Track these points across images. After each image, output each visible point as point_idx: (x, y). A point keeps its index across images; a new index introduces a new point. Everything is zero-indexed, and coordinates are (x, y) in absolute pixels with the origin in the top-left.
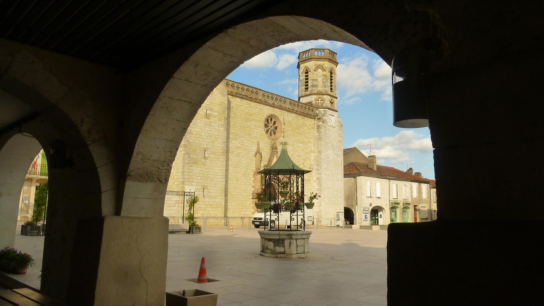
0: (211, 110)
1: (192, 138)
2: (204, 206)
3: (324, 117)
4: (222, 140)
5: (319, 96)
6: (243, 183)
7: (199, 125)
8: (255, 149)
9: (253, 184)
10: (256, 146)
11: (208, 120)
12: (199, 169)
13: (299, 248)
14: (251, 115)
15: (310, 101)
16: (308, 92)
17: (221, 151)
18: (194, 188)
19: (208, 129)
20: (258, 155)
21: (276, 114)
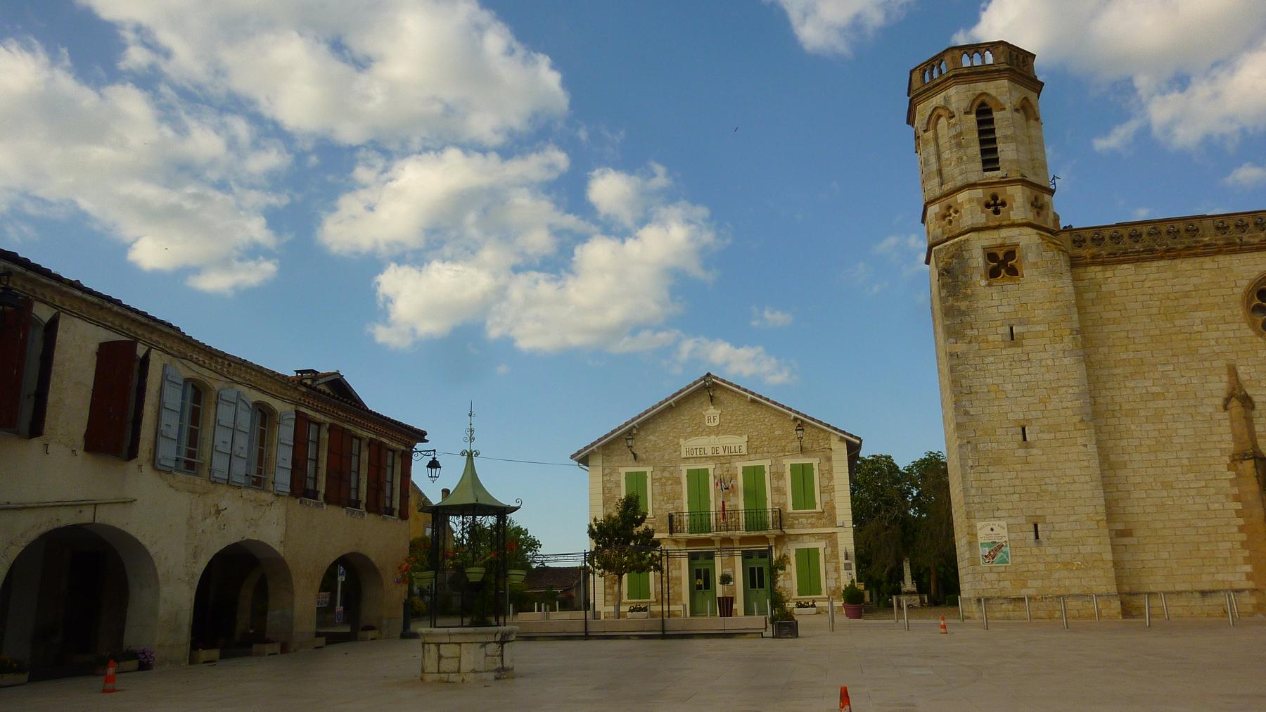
1: (976, 403)
2: (1041, 567)
4: (1076, 390)
6: (1193, 492)
7: (991, 367)
8: (1220, 386)
9: (1235, 491)
10: (1225, 378)
11: (1019, 350)
12: (1013, 475)
13: (443, 661)
14: (1187, 295)
17: (1077, 419)
18: (1004, 523)
19: (1021, 372)
20: (1234, 403)
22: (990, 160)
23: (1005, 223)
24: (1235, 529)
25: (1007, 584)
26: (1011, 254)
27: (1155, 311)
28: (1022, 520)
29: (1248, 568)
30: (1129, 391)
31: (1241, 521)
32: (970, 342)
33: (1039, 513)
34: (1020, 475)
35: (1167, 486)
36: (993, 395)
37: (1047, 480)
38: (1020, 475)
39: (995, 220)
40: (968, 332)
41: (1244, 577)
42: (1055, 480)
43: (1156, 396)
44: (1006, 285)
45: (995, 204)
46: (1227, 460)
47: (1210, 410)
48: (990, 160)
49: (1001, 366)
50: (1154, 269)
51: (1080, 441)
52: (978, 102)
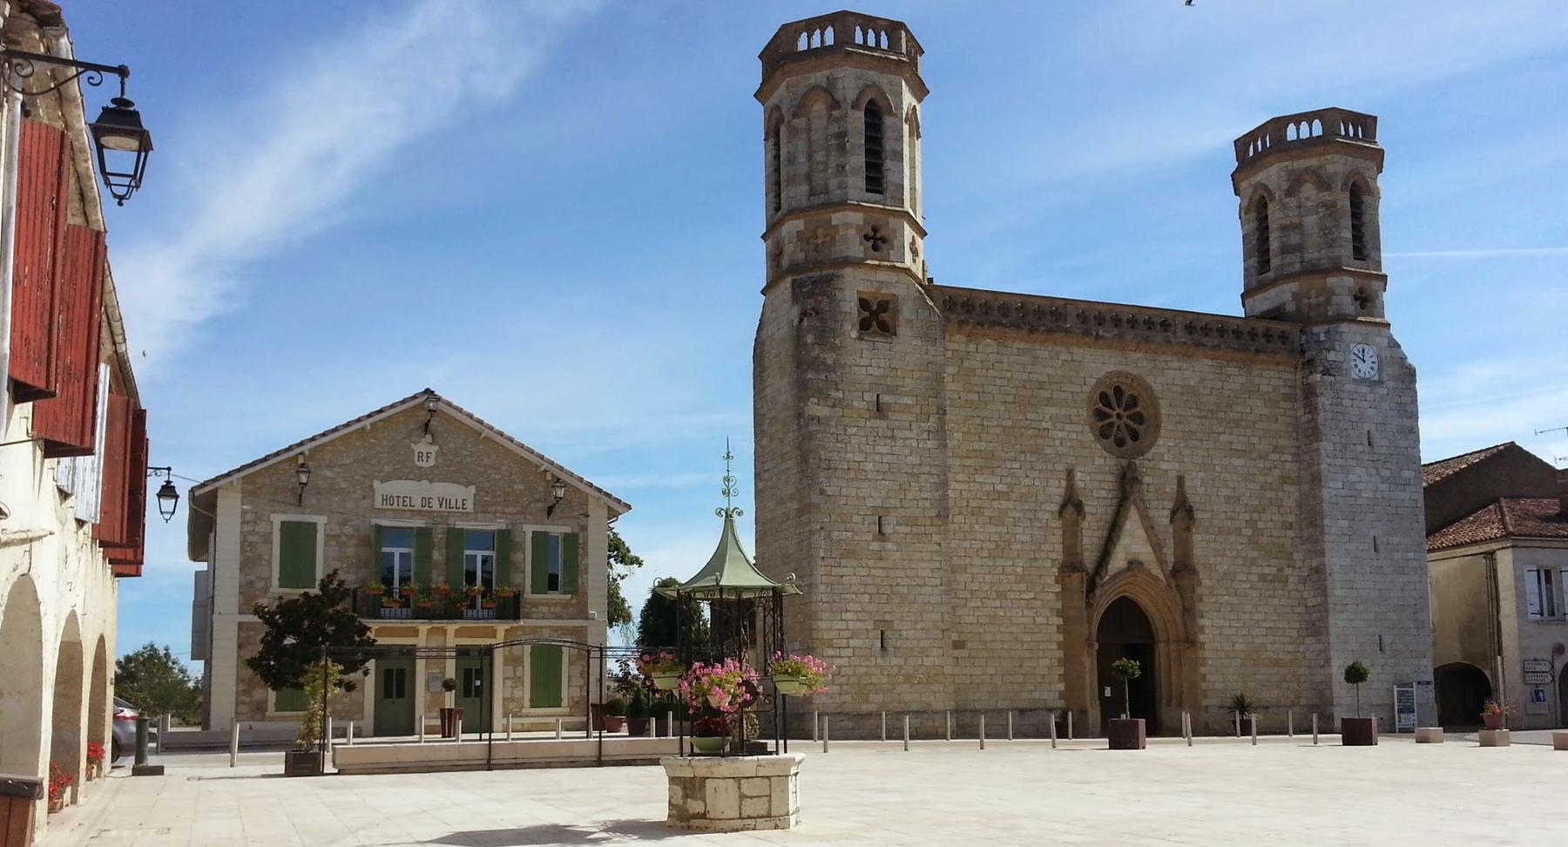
0: (892, 390)
2: (884, 680)
3: (1332, 356)
7: (854, 441)
8: (1057, 490)
10: (1064, 483)
11: (884, 424)
15: (1276, 303)
16: (1270, 275)
19: (885, 450)
20: (1070, 509)
24: (1055, 646)
25: (848, 698)
32: (834, 406)
35: (1001, 595)
36: (852, 474)
40: (834, 394)
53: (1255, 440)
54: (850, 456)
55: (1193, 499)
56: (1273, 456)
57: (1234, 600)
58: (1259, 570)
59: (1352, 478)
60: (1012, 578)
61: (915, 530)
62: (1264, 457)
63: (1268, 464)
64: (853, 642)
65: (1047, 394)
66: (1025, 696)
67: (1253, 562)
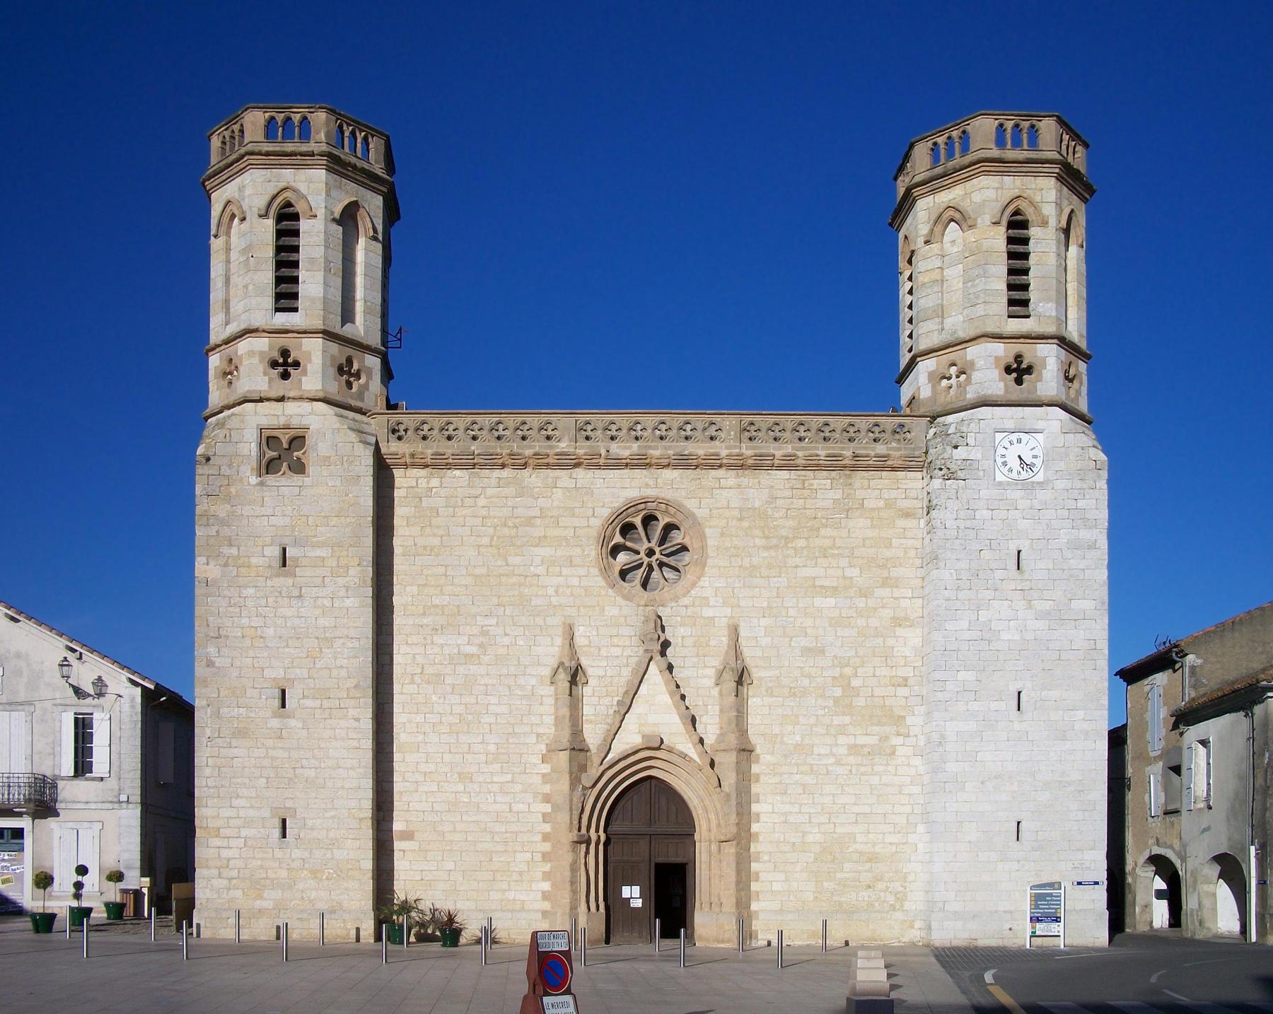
1: (225, 651)
2: (284, 873)
5: (946, 358)
7: (249, 603)
8: (551, 651)
11: (290, 581)
14: (529, 522)
17: (351, 683)
19: (289, 612)
21: (667, 494)
22: (1018, 302)
23: (292, 394)
24: (539, 838)
25: (239, 893)
26: (298, 441)
27: (486, 541)
28: (266, 813)
29: (546, 886)
30: (436, 650)
31: (547, 828)
32: (226, 565)
33: (289, 804)
34: (272, 753)
35: (465, 777)
36: (248, 642)
37: (304, 762)
38: (272, 753)
39: (1017, 393)
40: (227, 551)
41: (539, 896)
42: (313, 762)
43: (469, 656)
44: (284, 482)
45: (285, 364)
46: (543, 748)
47: (533, 681)
48: (1018, 302)
49: (263, 602)
50: (494, 482)
51: (352, 712)
52: (1011, 208)
53: (854, 572)
54: (245, 621)
55: (750, 654)
56: (879, 592)
57: (809, 780)
58: (851, 740)
59: (984, 615)
60: (483, 757)
61: (326, 704)
62: (864, 593)
63: (871, 602)
64: (244, 833)
65: (538, 532)
66: (495, 896)
67: (842, 730)
